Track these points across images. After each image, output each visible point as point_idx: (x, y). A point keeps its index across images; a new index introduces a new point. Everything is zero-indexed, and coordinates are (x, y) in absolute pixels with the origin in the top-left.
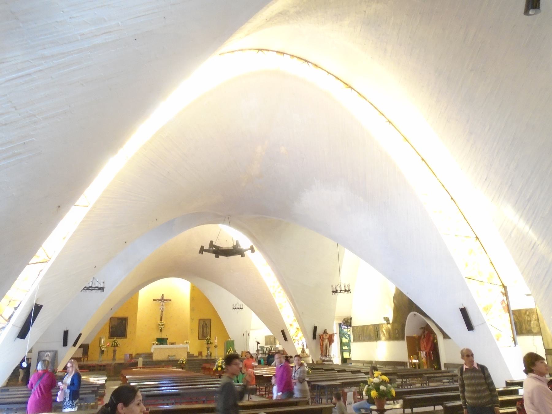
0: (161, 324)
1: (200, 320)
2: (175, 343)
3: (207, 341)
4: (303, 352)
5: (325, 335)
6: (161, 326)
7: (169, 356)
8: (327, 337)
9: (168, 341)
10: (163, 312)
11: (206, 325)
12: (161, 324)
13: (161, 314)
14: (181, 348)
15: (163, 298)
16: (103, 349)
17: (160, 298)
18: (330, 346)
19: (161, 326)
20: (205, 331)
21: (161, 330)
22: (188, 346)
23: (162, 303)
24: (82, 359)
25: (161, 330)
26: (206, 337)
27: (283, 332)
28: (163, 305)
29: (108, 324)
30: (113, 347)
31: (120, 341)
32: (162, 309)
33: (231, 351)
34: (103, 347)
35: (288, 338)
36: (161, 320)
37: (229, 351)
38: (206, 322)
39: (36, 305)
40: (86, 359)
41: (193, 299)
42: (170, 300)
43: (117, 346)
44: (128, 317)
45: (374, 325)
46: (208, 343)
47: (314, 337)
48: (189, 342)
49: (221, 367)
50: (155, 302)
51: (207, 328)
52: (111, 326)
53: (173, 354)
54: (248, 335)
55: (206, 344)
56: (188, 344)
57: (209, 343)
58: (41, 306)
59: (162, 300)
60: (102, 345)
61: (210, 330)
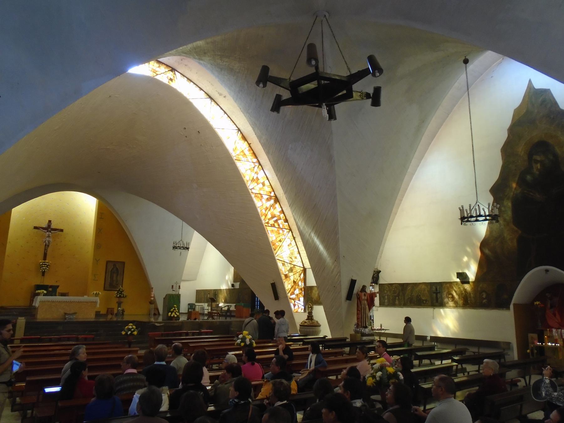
0: (45, 264)
1: (108, 262)
4: (310, 317)
5: (363, 293)
6: (44, 268)
7: (66, 314)
8: (366, 298)
9: (59, 290)
10: (48, 246)
11: (117, 269)
12: (45, 264)
13: (46, 250)
17: (45, 225)
18: (369, 311)
19: (44, 268)
20: (115, 278)
22: (98, 299)
23: (47, 233)
27: (273, 286)
28: (49, 236)
33: (175, 311)
35: (280, 295)
36: (45, 258)
37: (172, 310)
38: (117, 267)
42: (62, 230)
45: (214, 290)
46: (120, 297)
47: (349, 297)
48: (100, 293)
49: (554, 395)
50: (36, 230)
53: (72, 312)
54: (178, 287)
55: (117, 297)
57: (121, 295)
59: (49, 228)
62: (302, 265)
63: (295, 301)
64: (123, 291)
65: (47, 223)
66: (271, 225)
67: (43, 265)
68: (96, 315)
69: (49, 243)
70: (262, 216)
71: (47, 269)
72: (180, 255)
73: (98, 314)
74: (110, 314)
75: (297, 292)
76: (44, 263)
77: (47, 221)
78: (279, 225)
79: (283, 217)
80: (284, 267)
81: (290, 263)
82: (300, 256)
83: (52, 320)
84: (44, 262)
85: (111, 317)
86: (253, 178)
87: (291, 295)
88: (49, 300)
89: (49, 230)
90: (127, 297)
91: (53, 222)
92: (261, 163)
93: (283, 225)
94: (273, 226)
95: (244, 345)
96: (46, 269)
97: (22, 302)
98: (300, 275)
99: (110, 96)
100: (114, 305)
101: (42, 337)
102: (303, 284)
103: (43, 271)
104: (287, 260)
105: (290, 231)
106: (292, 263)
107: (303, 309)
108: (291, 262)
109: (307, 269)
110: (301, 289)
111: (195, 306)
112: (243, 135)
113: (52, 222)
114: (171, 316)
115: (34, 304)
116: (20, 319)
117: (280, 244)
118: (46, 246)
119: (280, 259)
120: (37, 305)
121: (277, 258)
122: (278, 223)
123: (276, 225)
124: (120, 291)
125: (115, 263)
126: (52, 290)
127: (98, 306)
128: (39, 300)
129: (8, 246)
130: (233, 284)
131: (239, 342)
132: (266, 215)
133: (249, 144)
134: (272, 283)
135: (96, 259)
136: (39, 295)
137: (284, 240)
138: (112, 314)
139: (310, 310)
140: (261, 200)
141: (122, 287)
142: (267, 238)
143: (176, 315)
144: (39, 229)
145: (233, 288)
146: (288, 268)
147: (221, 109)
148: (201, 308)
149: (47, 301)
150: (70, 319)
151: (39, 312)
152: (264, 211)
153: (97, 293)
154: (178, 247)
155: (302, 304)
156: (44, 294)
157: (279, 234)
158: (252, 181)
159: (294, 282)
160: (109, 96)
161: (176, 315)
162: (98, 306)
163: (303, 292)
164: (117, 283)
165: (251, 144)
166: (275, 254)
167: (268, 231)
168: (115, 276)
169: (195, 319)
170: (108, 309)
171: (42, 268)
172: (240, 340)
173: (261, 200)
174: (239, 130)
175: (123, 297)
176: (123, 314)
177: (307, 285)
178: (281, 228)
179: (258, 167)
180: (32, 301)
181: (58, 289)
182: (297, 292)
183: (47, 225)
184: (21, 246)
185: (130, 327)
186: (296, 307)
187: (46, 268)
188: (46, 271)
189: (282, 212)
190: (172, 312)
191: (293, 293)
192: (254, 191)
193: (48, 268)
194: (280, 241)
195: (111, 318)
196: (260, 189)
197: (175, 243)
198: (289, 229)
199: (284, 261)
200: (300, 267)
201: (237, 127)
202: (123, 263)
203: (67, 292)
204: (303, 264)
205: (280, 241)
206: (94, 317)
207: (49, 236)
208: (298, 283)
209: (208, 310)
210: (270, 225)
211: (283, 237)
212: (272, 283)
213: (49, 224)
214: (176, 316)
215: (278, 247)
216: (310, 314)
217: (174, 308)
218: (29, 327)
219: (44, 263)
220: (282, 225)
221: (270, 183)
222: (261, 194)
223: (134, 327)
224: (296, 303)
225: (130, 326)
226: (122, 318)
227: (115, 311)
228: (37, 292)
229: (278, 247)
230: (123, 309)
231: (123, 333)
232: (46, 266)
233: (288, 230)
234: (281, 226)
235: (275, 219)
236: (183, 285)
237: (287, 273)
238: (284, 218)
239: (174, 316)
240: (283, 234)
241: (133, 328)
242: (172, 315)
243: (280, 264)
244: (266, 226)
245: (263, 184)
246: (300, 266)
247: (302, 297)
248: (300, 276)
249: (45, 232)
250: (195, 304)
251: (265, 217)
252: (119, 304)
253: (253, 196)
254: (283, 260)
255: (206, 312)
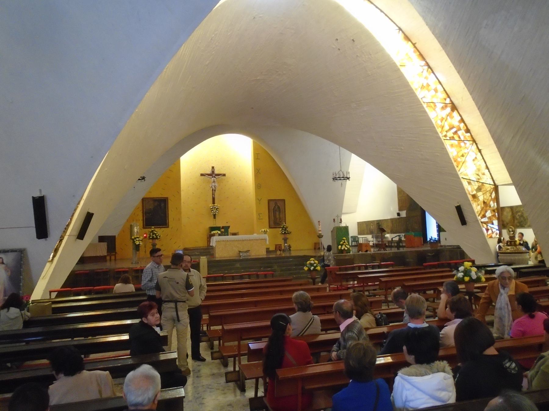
0: (214, 208)
1: (269, 201)
2: (238, 233)
3: (282, 230)
4: (513, 243)
7: (240, 251)
9: (230, 231)
10: (215, 190)
11: (279, 207)
12: (214, 208)
14: (256, 240)
15: (213, 172)
16: (137, 243)
17: (209, 172)
20: (278, 217)
21: (215, 216)
22: (266, 236)
23: (213, 179)
24: (108, 258)
25: (215, 216)
26: (280, 225)
27: (459, 209)
28: (214, 182)
29: (141, 208)
30: (151, 241)
31: (159, 231)
32: (213, 187)
33: (345, 244)
34: (137, 239)
36: (214, 203)
37: (341, 243)
39: (88, 213)
40: (113, 258)
41: (257, 171)
42: (224, 175)
43: (157, 238)
44: (167, 198)
45: (377, 221)
46: (285, 233)
48: (268, 230)
51: (280, 212)
52: (144, 211)
53: (245, 250)
55: (282, 234)
56: (266, 234)
57: (286, 232)
58: (92, 214)
59: (213, 174)
60: (136, 236)
61: (284, 215)
62: (493, 182)
63: (487, 225)
64: (287, 228)
65: (211, 170)
66: (450, 138)
67: (214, 209)
68: (266, 251)
69: (215, 187)
70: (438, 128)
71: (216, 212)
72: (342, 187)
73: (268, 251)
74: (279, 250)
75: (489, 214)
76: (213, 207)
77: (211, 168)
78: (459, 137)
79: (464, 127)
80: (470, 186)
81: (478, 181)
82: (489, 171)
83: (228, 258)
84: (214, 206)
85: (280, 253)
86: (423, 85)
87: (482, 218)
88: (233, 239)
89: (213, 175)
90: (291, 233)
91: (216, 168)
92: (431, 65)
93: (464, 137)
94: (452, 138)
95: (469, 280)
96: (216, 212)
97: (201, 243)
98: (491, 194)
99: (254, 17)
100: (280, 241)
101: (225, 275)
102: (496, 204)
103: (214, 214)
104: (473, 177)
105: (474, 143)
106: (480, 181)
107: (498, 234)
108: (479, 179)
109: (499, 186)
110: (494, 211)
111: (358, 238)
112: (405, 34)
113: (215, 168)
114: (341, 249)
115: (211, 245)
116: (202, 258)
117: (463, 159)
118: (213, 191)
119: (464, 177)
120: (214, 245)
121: (461, 176)
122: (458, 134)
123: (456, 137)
124: (284, 228)
125: (276, 201)
126: (225, 231)
127: (268, 242)
128: (214, 241)
129: (183, 193)
130: (399, 213)
131: (461, 277)
132: (443, 127)
133: (414, 45)
134: (456, 206)
135: (258, 199)
136: (215, 236)
137: (467, 154)
138: (280, 250)
139: (512, 234)
140: (434, 109)
141: (285, 224)
142: (447, 154)
143: (347, 247)
144: (205, 176)
145: (398, 217)
146: (476, 187)
147: (377, 7)
148: (364, 240)
149: (222, 241)
150: (245, 256)
151: (216, 252)
152: (439, 123)
153: (266, 230)
154: (339, 178)
155: (497, 228)
156: (218, 234)
157: (461, 147)
158: (422, 89)
159: (484, 202)
160: (253, 18)
161: (347, 247)
162: (268, 242)
163: (497, 214)
164: (280, 221)
165: (416, 43)
166: (458, 171)
167: (446, 145)
168: (277, 213)
169: (367, 251)
170: (276, 245)
171: (213, 211)
172: (462, 274)
173: (434, 109)
174: (400, 29)
175: (288, 233)
176: (290, 250)
177: (502, 205)
178: (462, 141)
179: (427, 71)
180: (209, 241)
181: (229, 230)
182: (489, 214)
183: (211, 171)
184: (193, 193)
185: (312, 262)
186: (490, 232)
187: (216, 211)
188: (216, 214)
189: (462, 120)
190: (342, 245)
191: (484, 216)
192: (424, 100)
193: (217, 211)
194: (463, 156)
195: (280, 254)
196: (433, 97)
197: (334, 174)
198: (472, 141)
199: (469, 179)
200: (490, 184)
201: (397, 26)
202: (284, 201)
203: (238, 232)
204: (493, 181)
205: (463, 156)
206: (266, 253)
207: (214, 182)
208: (489, 203)
209: (373, 241)
210: (449, 139)
211: (466, 151)
212: (458, 206)
213: (213, 170)
214: (346, 249)
215: (461, 163)
216: (512, 239)
217: (343, 241)
218: (213, 264)
219: (213, 207)
220: (463, 137)
221: (444, 88)
222: (434, 103)
223: (316, 262)
224: (489, 228)
225: (311, 261)
226: (290, 253)
227: (283, 248)
228: (212, 232)
229: (461, 163)
230: (289, 245)
231: (306, 268)
232: (216, 209)
233: (471, 142)
234: (462, 138)
235: (454, 130)
236: (344, 218)
237: (474, 192)
238: (465, 128)
239: (344, 249)
240: (466, 148)
241: (315, 263)
242: (343, 248)
243: (465, 183)
244: (444, 140)
245: (436, 91)
246: (491, 184)
247: (495, 219)
248: (491, 196)
249: (210, 178)
250: (357, 237)
251: (442, 129)
252: (285, 240)
253: (425, 106)
254: (469, 179)
255: (371, 244)
